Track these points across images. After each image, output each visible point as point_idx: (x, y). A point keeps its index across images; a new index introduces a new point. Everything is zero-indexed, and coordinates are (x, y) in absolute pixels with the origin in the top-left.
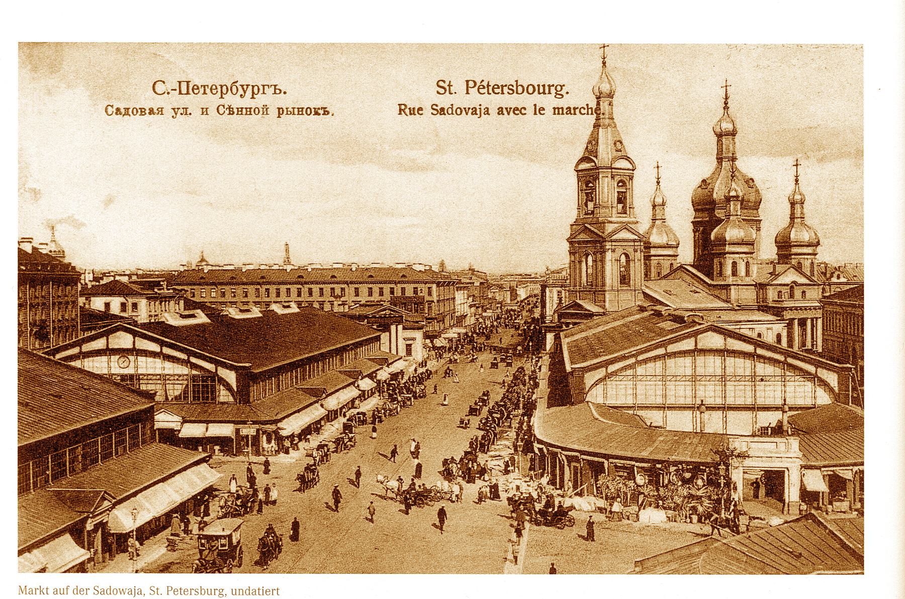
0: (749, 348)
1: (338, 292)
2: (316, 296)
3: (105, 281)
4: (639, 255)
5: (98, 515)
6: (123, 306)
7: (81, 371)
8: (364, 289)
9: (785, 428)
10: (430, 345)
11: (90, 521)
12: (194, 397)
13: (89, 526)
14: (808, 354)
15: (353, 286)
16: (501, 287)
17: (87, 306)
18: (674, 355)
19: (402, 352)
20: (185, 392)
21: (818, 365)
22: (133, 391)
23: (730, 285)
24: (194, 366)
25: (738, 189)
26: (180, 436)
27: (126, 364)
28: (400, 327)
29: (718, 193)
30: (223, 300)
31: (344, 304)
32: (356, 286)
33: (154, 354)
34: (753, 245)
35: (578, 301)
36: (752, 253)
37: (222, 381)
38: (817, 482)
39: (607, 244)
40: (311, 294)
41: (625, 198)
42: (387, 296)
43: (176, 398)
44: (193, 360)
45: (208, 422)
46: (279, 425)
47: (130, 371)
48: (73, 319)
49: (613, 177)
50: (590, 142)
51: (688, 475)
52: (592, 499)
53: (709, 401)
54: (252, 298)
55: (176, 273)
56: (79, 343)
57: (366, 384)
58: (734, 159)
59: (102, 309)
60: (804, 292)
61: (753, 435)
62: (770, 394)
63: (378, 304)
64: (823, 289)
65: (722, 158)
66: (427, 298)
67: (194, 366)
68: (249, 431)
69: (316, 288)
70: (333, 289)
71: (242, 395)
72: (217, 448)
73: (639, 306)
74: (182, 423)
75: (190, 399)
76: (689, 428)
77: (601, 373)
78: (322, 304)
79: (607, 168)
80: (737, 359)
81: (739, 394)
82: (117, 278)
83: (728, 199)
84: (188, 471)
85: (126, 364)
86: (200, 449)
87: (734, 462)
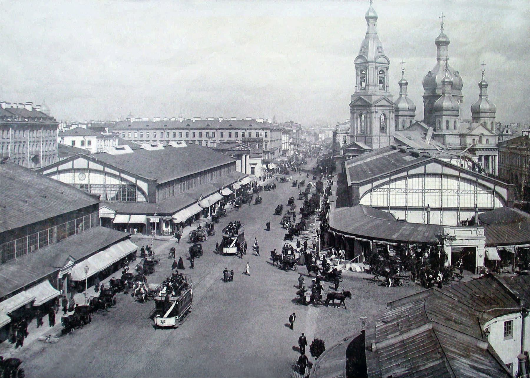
0: (456, 173)
1: (211, 134)
2: (197, 137)
3: (74, 127)
4: (392, 115)
5: (65, 269)
6: (83, 143)
7: (57, 182)
8: (226, 133)
9: (476, 222)
10: (266, 168)
11: (60, 273)
12: (123, 199)
13: (60, 276)
14: (491, 177)
15: (219, 131)
16: (309, 134)
17: (62, 143)
18: (413, 176)
19: (249, 172)
20: (117, 195)
21: (496, 184)
22: (87, 194)
23: (444, 135)
24: (122, 179)
25: (450, 78)
26: (114, 222)
27: (83, 178)
28: (248, 157)
29: (439, 79)
30: (141, 139)
31: (214, 142)
32: (222, 131)
33: (99, 172)
34: (458, 111)
35: (356, 142)
36: (458, 116)
37: (140, 189)
38: (494, 254)
39: (373, 108)
40: (194, 136)
41: (384, 81)
42: (240, 138)
43: (112, 199)
44: (123, 175)
45: (130, 214)
46: (174, 216)
47: (85, 182)
48: (54, 151)
49: (376, 68)
50: (363, 47)
51: (419, 250)
52: (362, 265)
53: (432, 205)
54: (159, 138)
55: (114, 123)
56: (57, 165)
57: (227, 192)
58: (447, 60)
59: (71, 144)
60: (487, 140)
61: (458, 226)
62: (467, 201)
63: (235, 142)
64: (499, 139)
65: (440, 59)
66: (264, 139)
67: (122, 179)
68: (155, 220)
69: (197, 132)
70: (207, 133)
71: (151, 198)
72: (136, 230)
73: (392, 146)
74: (116, 214)
75: (121, 199)
76: (420, 221)
77: (369, 186)
78: (200, 142)
79: (373, 62)
80: (449, 180)
81: (450, 201)
82: (80, 126)
83: (444, 83)
84: (118, 245)
85: (83, 178)
86: (126, 230)
87: (446, 242)
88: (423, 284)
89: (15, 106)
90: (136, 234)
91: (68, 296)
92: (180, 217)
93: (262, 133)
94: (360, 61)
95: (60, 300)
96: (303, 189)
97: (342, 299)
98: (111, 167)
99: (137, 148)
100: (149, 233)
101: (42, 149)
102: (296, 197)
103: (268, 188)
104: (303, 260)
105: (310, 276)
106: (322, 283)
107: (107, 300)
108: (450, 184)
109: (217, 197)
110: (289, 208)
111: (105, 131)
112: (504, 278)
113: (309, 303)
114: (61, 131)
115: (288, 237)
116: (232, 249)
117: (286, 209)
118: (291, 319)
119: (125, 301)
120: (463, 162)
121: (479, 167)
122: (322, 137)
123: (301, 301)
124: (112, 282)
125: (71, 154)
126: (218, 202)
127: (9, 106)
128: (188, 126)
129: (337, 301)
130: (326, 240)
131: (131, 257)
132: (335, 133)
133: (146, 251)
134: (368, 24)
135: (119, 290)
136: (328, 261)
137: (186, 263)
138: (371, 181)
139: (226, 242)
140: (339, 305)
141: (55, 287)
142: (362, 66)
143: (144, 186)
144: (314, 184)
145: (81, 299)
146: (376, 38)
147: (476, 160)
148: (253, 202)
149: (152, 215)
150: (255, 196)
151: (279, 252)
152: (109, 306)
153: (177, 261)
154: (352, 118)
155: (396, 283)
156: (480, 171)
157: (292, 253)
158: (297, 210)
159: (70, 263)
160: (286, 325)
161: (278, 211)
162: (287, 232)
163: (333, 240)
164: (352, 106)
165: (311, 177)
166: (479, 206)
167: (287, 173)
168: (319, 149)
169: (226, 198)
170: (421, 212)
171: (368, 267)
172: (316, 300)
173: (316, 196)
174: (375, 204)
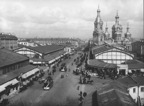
0: (120, 51)
1: (58, 42)
3: (22, 40)
4: (104, 36)
6: (25, 44)
8: (62, 41)
13: (19, 77)
14: (130, 52)
18: (104, 53)
19: (67, 51)
20: (34, 57)
21: (131, 53)
29: (116, 27)
31: (59, 43)
38: (130, 71)
42: (65, 42)
45: (37, 61)
47: (25, 53)
51: (111, 70)
53: (114, 59)
54: (44, 42)
57: (62, 56)
58: (118, 22)
61: (121, 64)
62: (123, 58)
67: (35, 53)
68: (44, 63)
71: (43, 57)
76: (111, 63)
77: (98, 54)
78: (55, 43)
81: (119, 58)
83: (117, 28)
87: (118, 68)
88: (112, 79)
89: (6, 34)
90: (39, 67)
91: (21, 82)
92: (50, 62)
93: (71, 41)
94: (95, 23)
95: (19, 83)
96: (81, 55)
97: (91, 82)
98: (32, 50)
99: (39, 45)
100: (42, 66)
101: (14, 45)
102: (79, 57)
103: (72, 55)
104: (81, 73)
105: (83, 77)
106: (86, 78)
107: (32, 83)
108: (119, 54)
109: (59, 57)
110: (78, 60)
111: (30, 41)
112: (133, 77)
113: (82, 83)
114: (19, 41)
115: (77, 67)
116: (63, 70)
117: (77, 60)
118: (78, 87)
119: (36, 83)
120: (122, 48)
121: (126, 49)
122: (86, 42)
123: (80, 83)
124: (33, 79)
125: (22, 46)
126: (60, 58)
127: (4, 34)
128: (52, 39)
129: (90, 83)
130: (87, 67)
131: (38, 72)
132: (89, 41)
133: (41, 71)
134: (98, 13)
135: (35, 81)
136: (87, 73)
137: (52, 74)
138: (98, 53)
139: (62, 68)
140: (90, 84)
141: (18, 80)
142: (96, 24)
143: (41, 54)
144: (84, 54)
145: (25, 83)
146: (100, 17)
147: (125, 47)
148: (69, 58)
149: (43, 62)
150: (69, 57)
151: (75, 71)
152: (32, 85)
153: (50, 73)
154: (93, 37)
155: (105, 78)
156: (127, 50)
157: (78, 71)
158: (80, 60)
159: (22, 74)
160: (77, 89)
161: (75, 61)
162: (77, 66)
163: (88, 68)
164: (93, 34)
165: (83, 52)
166: (126, 59)
167: (77, 51)
168: (85, 45)
169: (62, 58)
170: (111, 61)
171: (97, 74)
172: (84, 83)
173: (84, 57)
174: (99, 59)
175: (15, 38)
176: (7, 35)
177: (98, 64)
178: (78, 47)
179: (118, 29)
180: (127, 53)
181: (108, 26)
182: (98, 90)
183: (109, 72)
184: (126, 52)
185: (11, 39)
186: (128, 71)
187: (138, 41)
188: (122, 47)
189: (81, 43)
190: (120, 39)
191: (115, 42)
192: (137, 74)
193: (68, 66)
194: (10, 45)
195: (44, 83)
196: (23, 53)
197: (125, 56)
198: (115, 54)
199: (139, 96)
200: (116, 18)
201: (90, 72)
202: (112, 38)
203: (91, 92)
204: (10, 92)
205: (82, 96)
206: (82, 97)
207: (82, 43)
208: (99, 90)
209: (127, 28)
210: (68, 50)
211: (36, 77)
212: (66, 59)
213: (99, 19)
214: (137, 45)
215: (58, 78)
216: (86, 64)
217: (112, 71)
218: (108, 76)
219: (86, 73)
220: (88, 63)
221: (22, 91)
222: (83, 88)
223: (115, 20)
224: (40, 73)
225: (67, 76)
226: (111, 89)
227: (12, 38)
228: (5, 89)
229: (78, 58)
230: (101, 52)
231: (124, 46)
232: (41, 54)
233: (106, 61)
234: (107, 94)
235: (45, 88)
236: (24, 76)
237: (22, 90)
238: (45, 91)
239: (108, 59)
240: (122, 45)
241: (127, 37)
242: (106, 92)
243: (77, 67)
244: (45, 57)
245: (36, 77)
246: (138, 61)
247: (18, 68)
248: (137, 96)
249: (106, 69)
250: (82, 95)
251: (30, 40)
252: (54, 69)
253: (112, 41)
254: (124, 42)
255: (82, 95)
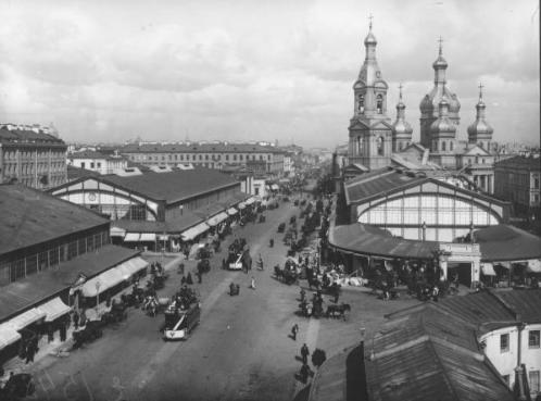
0: (452, 192)
1: (216, 157)
3: (83, 149)
4: (389, 138)
6: (92, 165)
8: (231, 156)
13: (71, 292)
14: (488, 196)
19: (253, 192)
20: (128, 215)
21: (491, 202)
29: (435, 102)
31: (220, 164)
38: (489, 269)
42: (245, 160)
45: (141, 233)
47: (96, 202)
51: (415, 265)
53: (428, 223)
54: (167, 160)
57: (232, 211)
58: (444, 83)
61: (453, 243)
62: (463, 219)
67: (132, 200)
68: (164, 238)
71: (160, 216)
76: (416, 238)
77: (367, 205)
78: (207, 164)
81: (446, 219)
83: (441, 106)
87: (442, 258)
88: (419, 298)
89: (21, 128)
90: (146, 252)
91: (79, 311)
92: (189, 235)
93: (265, 156)
94: (359, 86)
95: (72, 316)
96: (304, 208)
97: (342, 312)
98: (121, 188)
99: (145, 170)
100: (158, 250)
101: (51, 170)
102: (298, 215)
103: (271, 207)
104: (304, 275)
105: (311, 290)
106: (323, 296)
107: (119, 315)
108: (446, 202)
109: (223, 216)
110: (291, 226)
111: (114, 154)
112: (500, 293)
113: (310, 316)
114: (70, 154)
115: (291, 253)
116: (238, 265)
117: (288, 227)
118: (293, 331)
119: (136, 315)
120: (459, 182)
121: (475, 186)
122: (322, 159)
123: (302, 313)
124: (123, 297)
125: (82, 175)
126: (224, 221)
127: (15, 128)
128: (195, 149)
129: (337, 313)
130: (326, 255)
131: (141, 273)
132: (335, 156)
133: (155, 268)
134: (367, 50)
135: (130, 305)
136: (328, 276)
137: (195, 279)
138: (369, 201)
139: (233, 259)
140: (338, 317)
141: (66, 303)
142: (361, 91)
143: (153, 206)
144: (314, 204)
145: (92, 315)
146: (375, 63)
147: (471, 179)
148: (257, 220)
149: (161, 233)
150: (259, 215)
151: (282, 267)
152: (120, 320)
153: (186, 276)
154: (351, 141)
155: (393, 296)
156: (476, 190)
157: (294, 269)
158: (299, 228)
159: (81, 280)
160: (290, 336)
161: (281, 229)
162: (289, 248)
163: (331, 256)
164: (351, 129)
165: (312, 197)
166: (475, 223)
167: (289, 193)
168: (319, 170)
169: (231, 218)
170: (416, 230)
171: (366, 281)
172: (317, 313)
173: (316, 215)
174: (373, 222)
175: (56, 144)
176: (28, 134)
177: (369, 242)
178: (294, 178)
179: (445, 110)
180: (476, 200)
181: (406, 97)
182: (367, 339)
183: (410, 273)
184: (473, 195)
185: (41, 149)
186: (481, 268)
187: (517, 157)
188: (460, 177)
189: (305, 163)
190: (450, 149)
191: (430, 158)
192: (516, 282)
193: (255, 250)
194: (37, 171)
195: (167, 315)
196: (88, 202)
197: (471, 210)
198: (434, 206)
199: (522, 362)
200: (436, 67)
201: (338, 271)
202: (422, 143)
203: (341, 349)
204: (37, 350)
205: (310, 363)
206: (308, 367)
207: (309, 161)
208: (371, 341)
209: (478, 108)
210: (257, 191)
211: (137, 291)
212: (249, 224)
213: (371, 71)
214: (517, 169)
215: (218, 295)
216: (321, 243)
217: (422, 270)
218: (405, 287)
219: (325, 276)
220: (331, 239)
221: (84, 345)
222: (312, 333)
223: (433, 77)
224: (149, 277)
225: (251, 287)
226: (416, 338)
227: (44, 144)
228: (19, 336)
229: (293, 220)
230: (379, 197)
231: (465, 175)
232: (153, 206)
233: (400, 229)
234: (400, 355)
235: (168, 334)
236: (90, 289)
237: (81, 341)
238: (169, 343)
239: (406, 222)
240: (458, 169)
241: (478, 142)
242: (398, 349)
243: (291, 253)
244: (169, 215)
245: (137, 291)
246: (519, 230)
247: (69, 258)
248: (516, 365)
249: (397, 262)
250: (309, 358)
251: (112, 152)
252: (203, 261)
253: (422, 156)
254: (465, 161)
255: (309, 358)
